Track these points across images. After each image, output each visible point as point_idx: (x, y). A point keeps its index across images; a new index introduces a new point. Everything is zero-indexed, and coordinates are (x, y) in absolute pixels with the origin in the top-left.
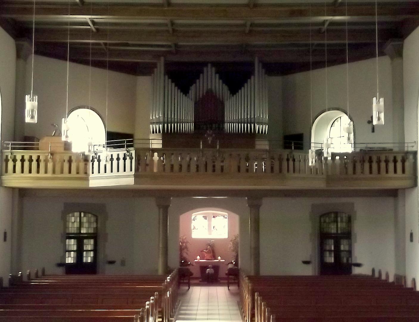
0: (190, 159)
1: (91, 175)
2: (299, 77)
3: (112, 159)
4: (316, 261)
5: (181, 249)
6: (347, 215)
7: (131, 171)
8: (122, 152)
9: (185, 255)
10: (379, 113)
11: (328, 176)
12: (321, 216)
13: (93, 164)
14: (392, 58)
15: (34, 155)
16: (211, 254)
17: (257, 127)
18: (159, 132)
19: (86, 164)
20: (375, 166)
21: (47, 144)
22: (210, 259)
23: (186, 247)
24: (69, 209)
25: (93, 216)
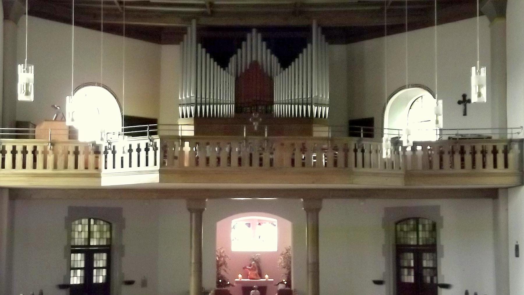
0: (230, 150)
3: (130, 151)
4: (390, 281)
5: (219, 266)
6: (430, 222)
7: (155, 165)
8: (143, 141)
9: (223, 273)
10: (480, 86)
11: (407, 171)
12: (397, 224)
13: (106, 157)
14: (491, 20)
15: (30, 145)
16: (256, 272)
17: (315, 109)
18: (191, 116)
19: (97, 157)
20: (468, 158)
21: (46, 132)
22: (255, 277)
23: (224, 263)
24: (75, 214)
25: (105, 223)
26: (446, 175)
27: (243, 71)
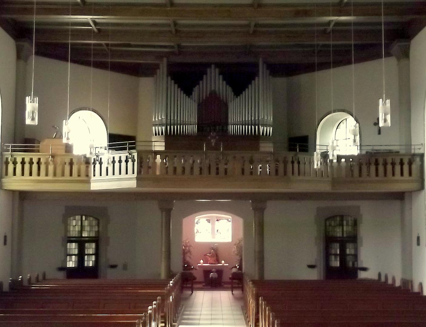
0: (194, 162)
1: (93, 178)
2: (304, 78)
3: (114, 162)
4: (321, 266)
5: (184, 253)
6: (353, 219)
7: (133, 173)
8: (124, 155)
9: (188, 259)
10: (385, 115)
11: (333, 179)
12: (326, 220)
13: (94, 167)
14: (399, 59)
15: (35, 157)
16: (215, 258)
17: (261, 129)
18: (162, 134)
19: (87, 167)
20: (381, 168)
21: (47, 146)
22: (214, 263)
23: (189, 251)
24: (70, 212)
25: (94, 219)
26: (362, 182)
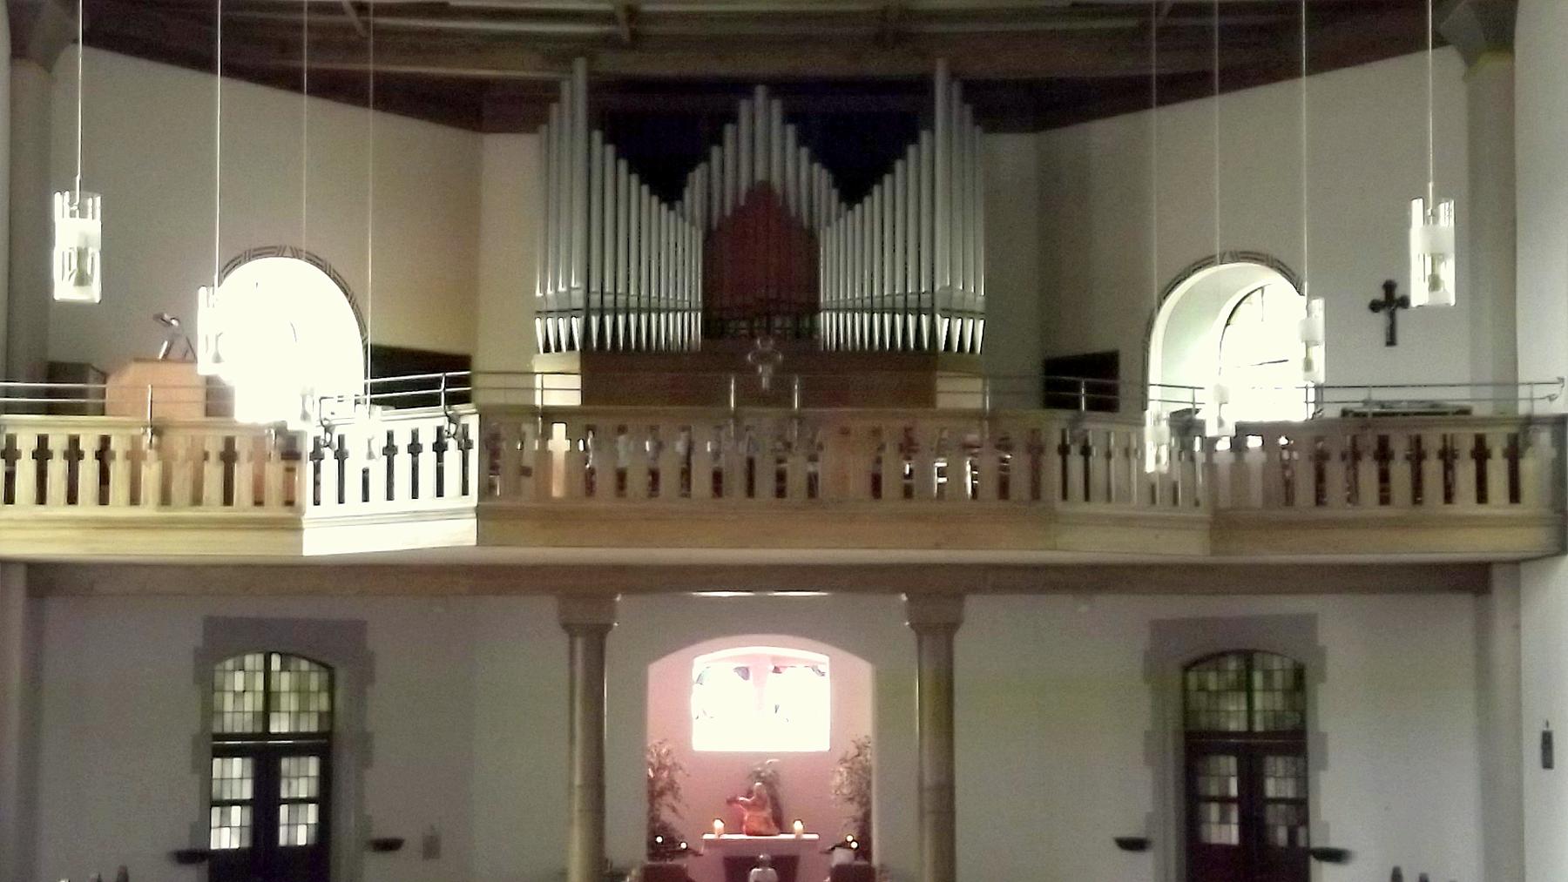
0: (689, 450)
3: (390, 450)
4: (1168, 841)
5: (655, 794)
6: (1288, 664)
7: (465, 492)
8: (427, 422)
9: (666, 815)
10: (1436, 258)
11: (1217, 512)
12: (1187, 669)
13: (317, 470)
14: (1470, 58)
15: (89, 434)
16: (767, 813)
17: (942, 326)
18: (571, 346)
19: (290, 470)
20: (1400, 471)
21: (138, 395)
22: (763, 829)
23: (672, 787)
24: (225, 640)
25: (315, 667)
26: (1335, 524)
27: (728, 212)
